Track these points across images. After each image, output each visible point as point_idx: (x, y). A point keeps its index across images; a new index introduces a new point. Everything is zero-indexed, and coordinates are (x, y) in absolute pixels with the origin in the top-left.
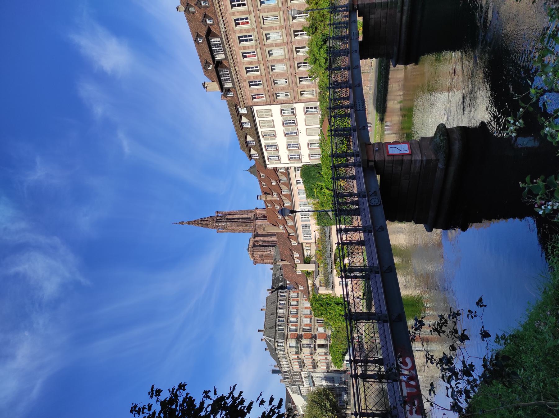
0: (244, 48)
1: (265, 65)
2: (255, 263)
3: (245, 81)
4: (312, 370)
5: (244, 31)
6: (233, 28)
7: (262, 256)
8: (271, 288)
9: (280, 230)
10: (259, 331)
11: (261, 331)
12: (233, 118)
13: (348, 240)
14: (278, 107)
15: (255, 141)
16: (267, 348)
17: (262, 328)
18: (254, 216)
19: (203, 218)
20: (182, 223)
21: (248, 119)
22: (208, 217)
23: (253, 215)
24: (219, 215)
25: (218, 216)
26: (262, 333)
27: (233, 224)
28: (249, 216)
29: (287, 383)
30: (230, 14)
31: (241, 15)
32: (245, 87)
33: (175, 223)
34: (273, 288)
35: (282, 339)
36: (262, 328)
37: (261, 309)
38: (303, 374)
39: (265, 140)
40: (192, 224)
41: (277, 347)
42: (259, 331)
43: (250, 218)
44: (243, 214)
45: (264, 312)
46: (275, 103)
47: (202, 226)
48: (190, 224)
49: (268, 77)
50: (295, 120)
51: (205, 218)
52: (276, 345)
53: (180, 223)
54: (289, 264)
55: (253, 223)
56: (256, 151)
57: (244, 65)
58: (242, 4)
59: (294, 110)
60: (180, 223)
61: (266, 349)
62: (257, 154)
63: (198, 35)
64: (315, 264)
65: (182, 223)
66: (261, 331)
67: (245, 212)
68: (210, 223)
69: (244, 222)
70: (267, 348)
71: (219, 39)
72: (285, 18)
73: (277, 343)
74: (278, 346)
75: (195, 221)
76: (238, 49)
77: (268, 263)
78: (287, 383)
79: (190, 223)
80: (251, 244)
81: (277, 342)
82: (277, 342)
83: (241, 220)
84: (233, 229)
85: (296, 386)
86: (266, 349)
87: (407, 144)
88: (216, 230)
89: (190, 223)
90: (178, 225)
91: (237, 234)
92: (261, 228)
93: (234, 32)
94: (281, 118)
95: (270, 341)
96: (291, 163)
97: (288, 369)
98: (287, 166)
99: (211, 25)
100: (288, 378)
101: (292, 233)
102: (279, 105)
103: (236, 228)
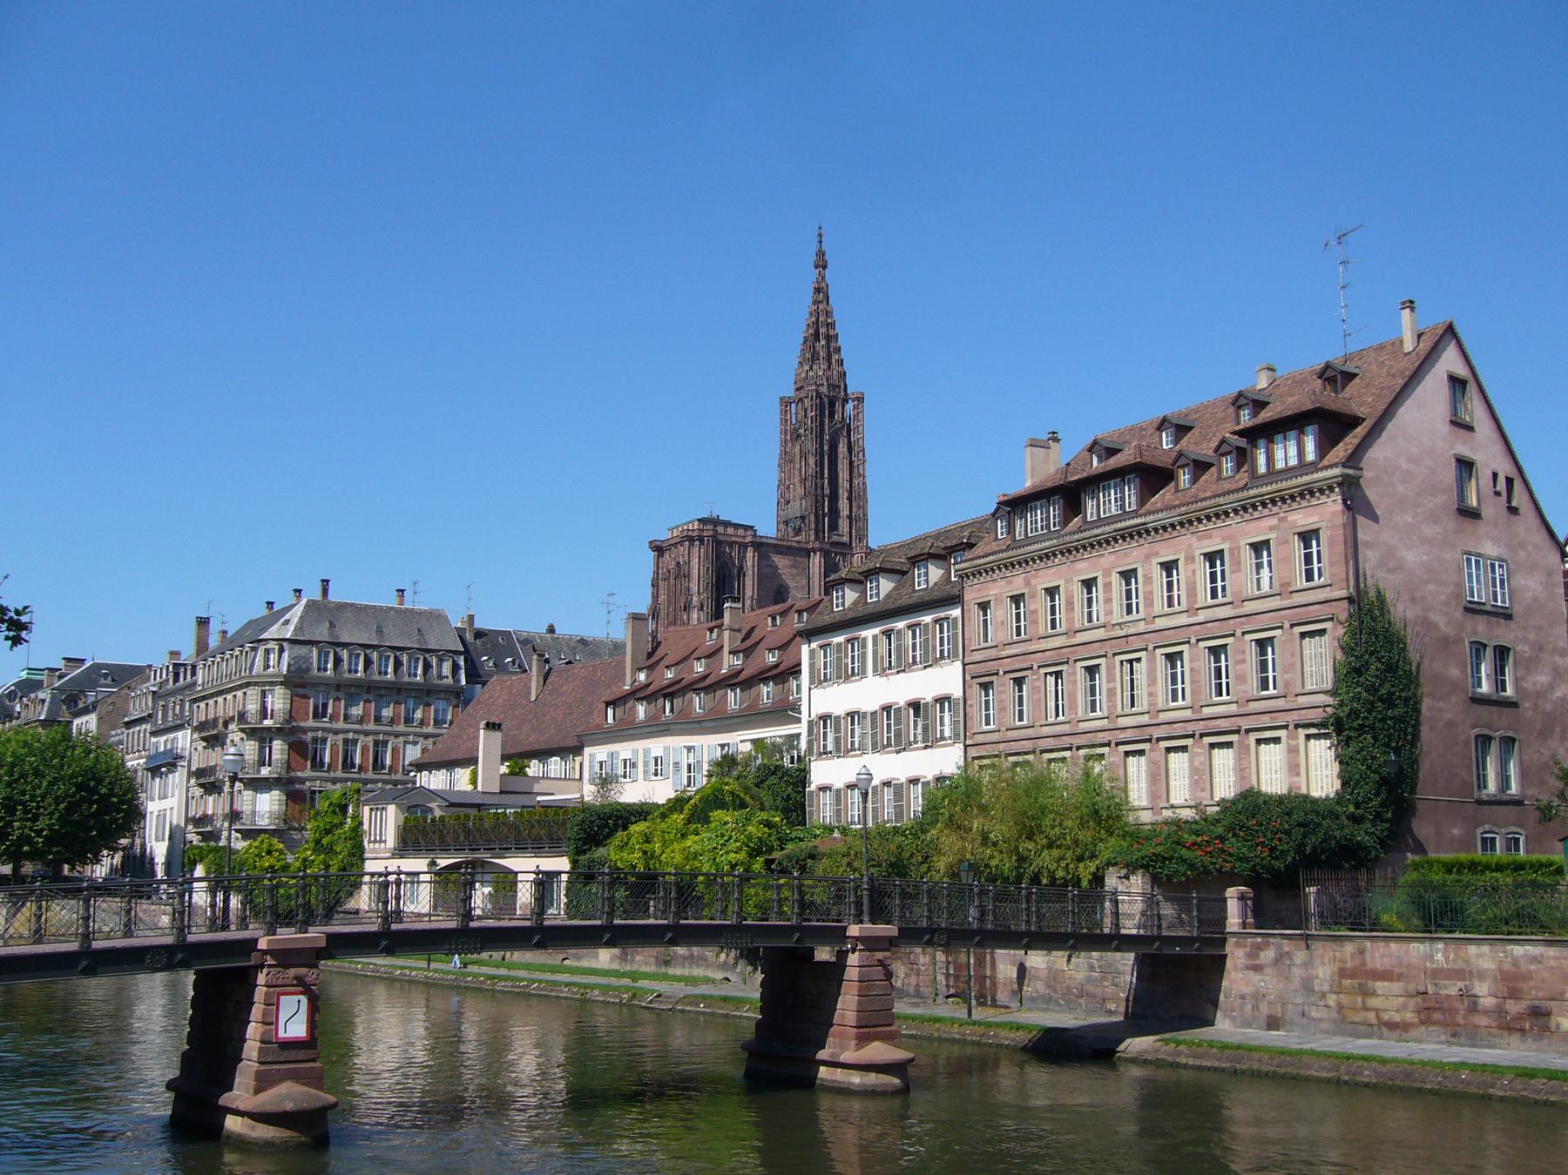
0: (1108, 586)
1: (1064, 650)
2: (659, 549)
3: (1027, 583)
4: (193, 769)
5: (1148, 589)
6: (1157, 554)
7: (681, 573)
8: (477, 625)
9: (633, 674)
10: (325, 582)
11: (325, 592)
12: (939, 535)
13: (375, 908)
14: (957, 693)
15: (879, 601)
16: (277, 608)
17: (335, 596)
18: (844, 544)
19: (840, 343)
20: (821, 264)
21: (935, 584)
22: (841, 362)
23: (846, 539)
24: (850, 406)
25: (845, 401)
26: (318, 596)
27: (812, 461)
28: (843, 525)
29: (164, 677)
30: (1190, 547)
31: (1187, 583)
32: (1011, 582)
33: (820, 235)
34: (479, 634)
35: (289, 665)
36: (335, 596)
37: (402, 591)
38: (184, 740)
39: (875, 637)
40: (816, 302)
41: (262, 648)
42: (325, 582)
43: (834, 527)
44: (849, 498)
45: (393, 602)
46: (968, 677)
47: (806, 340)
48: (818, 290)
49: (1034, 660)
50: (859, 749)
51: (838, 350)
52: (271, 645)
53: (821, 254)
54: (533, 699)
55: (812, 538)
56: (888, 596)
57: (1066, 582)
58: (1312, 569)
59: (858, 752)
60: (821, 254)
61: (270, 604)
62: (878, 595)
63: (1181, 430)
64: (502, 792)
65: (821, 264)
66: (325, 592)
67: (859, 507)
68: (820, 369)
69: (818, 503)
70: (277, 608)
71: (1134, 507)
72: (1175, 726)
73: (277, 647)
74: (267, 652)
75: (828, 314)
76: (1107, 566)
77: (655, 596)
78: (164, 677)
79: (821, 291)
80: (730, 531)
81: (282, 650)
82: (282, 650)
83: (827, 491)
84: (791, 461)
85: (153, 709)
86: (270, 604)
87: (305, 1035)
88: (790, 392)
89: (821, 291)
90: (814, 247)
91: (774, 476)
92: (794, 571)
93: (1148, 557)
94: (929, 699)
95: (287, 622)
96: (810, 723)
97: (200, 682)
98: (804, 709)
99: (1220, 471)
100: (176, 679)
101: (672, 710)
102: (961, 694)
103: (797, 472)
